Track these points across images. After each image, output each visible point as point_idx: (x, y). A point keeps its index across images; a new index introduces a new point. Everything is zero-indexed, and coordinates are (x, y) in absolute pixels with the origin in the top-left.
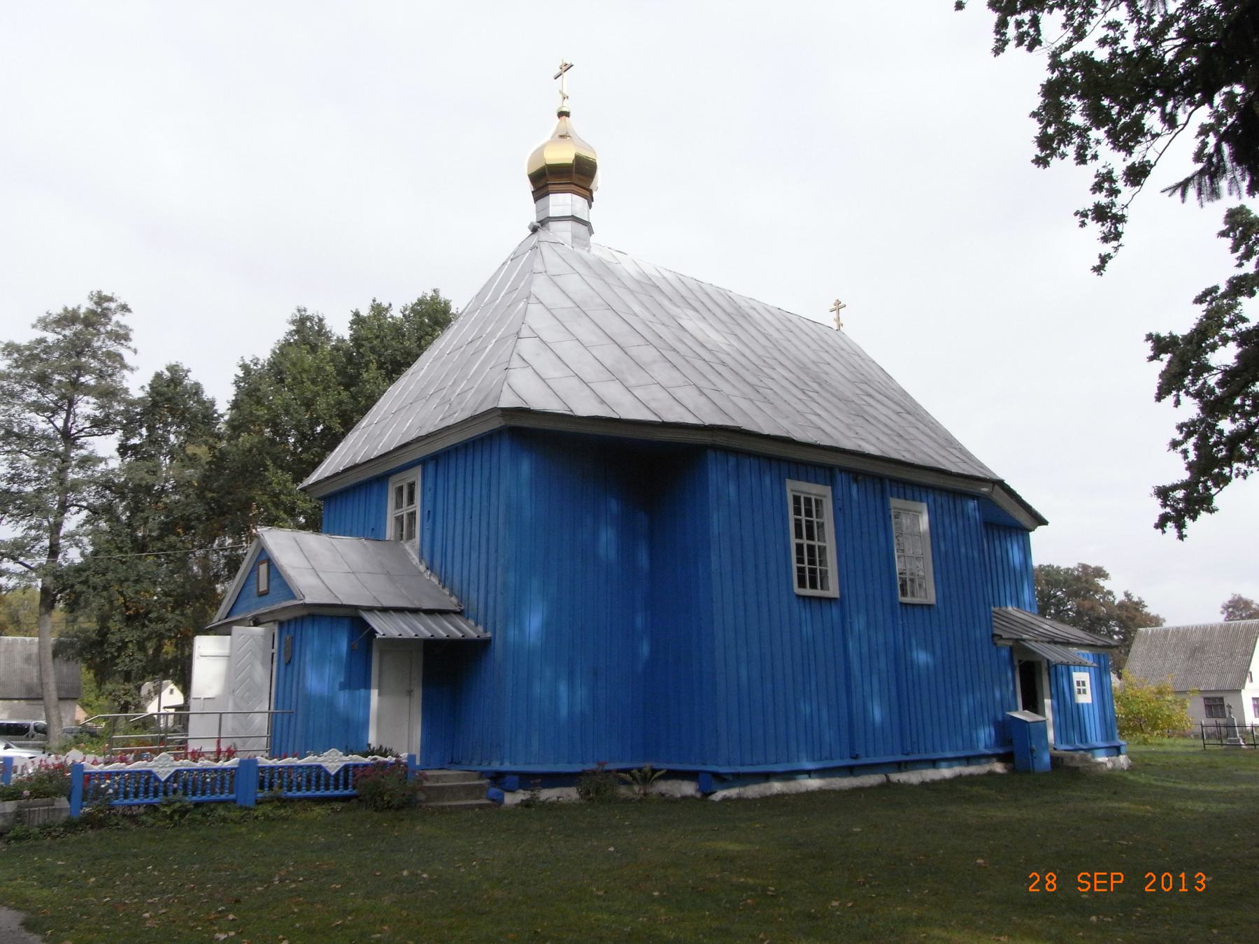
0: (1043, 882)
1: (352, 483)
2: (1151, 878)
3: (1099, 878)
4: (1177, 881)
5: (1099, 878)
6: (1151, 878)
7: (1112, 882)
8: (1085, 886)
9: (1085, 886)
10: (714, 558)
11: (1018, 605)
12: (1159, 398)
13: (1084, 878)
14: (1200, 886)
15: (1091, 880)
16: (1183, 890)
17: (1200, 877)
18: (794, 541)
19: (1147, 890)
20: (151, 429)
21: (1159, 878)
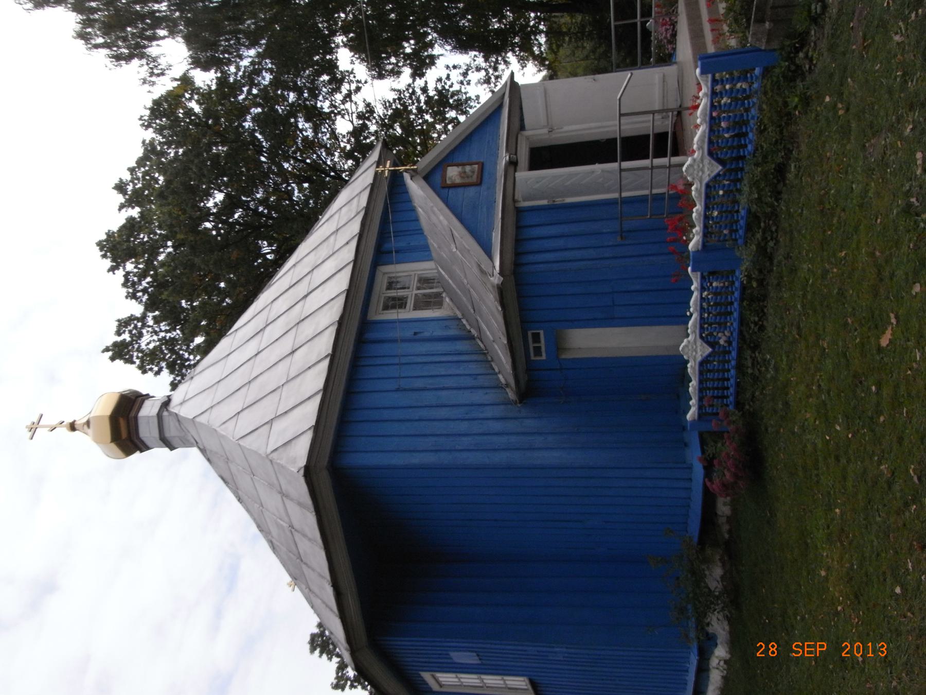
0: (767, 649)
1: (347, 365)
2: (761, 646)
3: (809, 646)
4: (865, 649)
5: (809, 646)
6: (761, 646)
7: (818, 649)
8: (798, 652)
9: (798, 652)
10: (416, 459)
11: (683, 165)
12: (103, 351)
13: (797, 646)
14: (882, 652)
15: (803, 648)
16: (870, 655)
17: (883, 646)
18: (408, 314)
19: (843, 655)
20: (251, 209)
21: (852, 647)
